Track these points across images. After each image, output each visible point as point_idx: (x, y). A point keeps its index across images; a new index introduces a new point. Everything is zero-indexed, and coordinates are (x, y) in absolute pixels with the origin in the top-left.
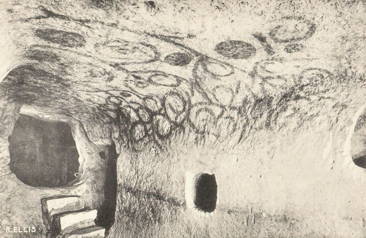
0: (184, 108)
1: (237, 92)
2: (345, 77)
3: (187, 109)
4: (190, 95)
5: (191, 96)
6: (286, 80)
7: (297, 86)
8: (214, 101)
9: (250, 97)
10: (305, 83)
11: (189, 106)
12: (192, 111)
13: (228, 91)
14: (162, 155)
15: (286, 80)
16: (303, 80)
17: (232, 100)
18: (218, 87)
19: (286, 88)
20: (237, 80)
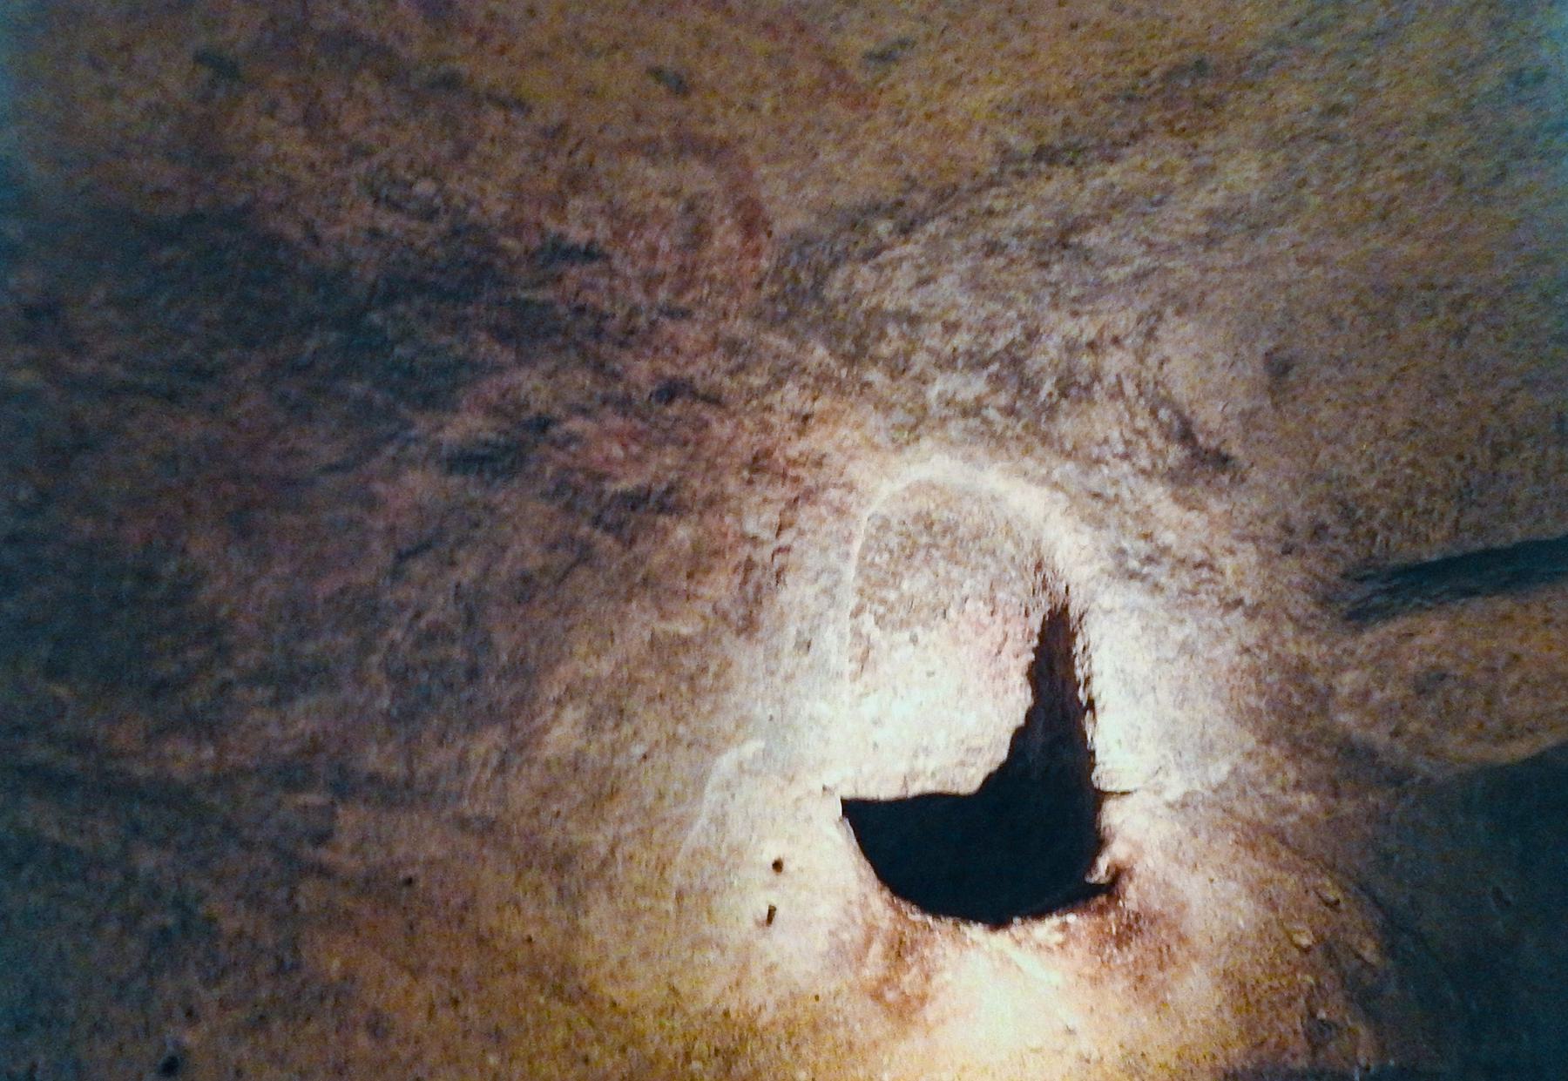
10: (577, 234)
15: (462, 153)
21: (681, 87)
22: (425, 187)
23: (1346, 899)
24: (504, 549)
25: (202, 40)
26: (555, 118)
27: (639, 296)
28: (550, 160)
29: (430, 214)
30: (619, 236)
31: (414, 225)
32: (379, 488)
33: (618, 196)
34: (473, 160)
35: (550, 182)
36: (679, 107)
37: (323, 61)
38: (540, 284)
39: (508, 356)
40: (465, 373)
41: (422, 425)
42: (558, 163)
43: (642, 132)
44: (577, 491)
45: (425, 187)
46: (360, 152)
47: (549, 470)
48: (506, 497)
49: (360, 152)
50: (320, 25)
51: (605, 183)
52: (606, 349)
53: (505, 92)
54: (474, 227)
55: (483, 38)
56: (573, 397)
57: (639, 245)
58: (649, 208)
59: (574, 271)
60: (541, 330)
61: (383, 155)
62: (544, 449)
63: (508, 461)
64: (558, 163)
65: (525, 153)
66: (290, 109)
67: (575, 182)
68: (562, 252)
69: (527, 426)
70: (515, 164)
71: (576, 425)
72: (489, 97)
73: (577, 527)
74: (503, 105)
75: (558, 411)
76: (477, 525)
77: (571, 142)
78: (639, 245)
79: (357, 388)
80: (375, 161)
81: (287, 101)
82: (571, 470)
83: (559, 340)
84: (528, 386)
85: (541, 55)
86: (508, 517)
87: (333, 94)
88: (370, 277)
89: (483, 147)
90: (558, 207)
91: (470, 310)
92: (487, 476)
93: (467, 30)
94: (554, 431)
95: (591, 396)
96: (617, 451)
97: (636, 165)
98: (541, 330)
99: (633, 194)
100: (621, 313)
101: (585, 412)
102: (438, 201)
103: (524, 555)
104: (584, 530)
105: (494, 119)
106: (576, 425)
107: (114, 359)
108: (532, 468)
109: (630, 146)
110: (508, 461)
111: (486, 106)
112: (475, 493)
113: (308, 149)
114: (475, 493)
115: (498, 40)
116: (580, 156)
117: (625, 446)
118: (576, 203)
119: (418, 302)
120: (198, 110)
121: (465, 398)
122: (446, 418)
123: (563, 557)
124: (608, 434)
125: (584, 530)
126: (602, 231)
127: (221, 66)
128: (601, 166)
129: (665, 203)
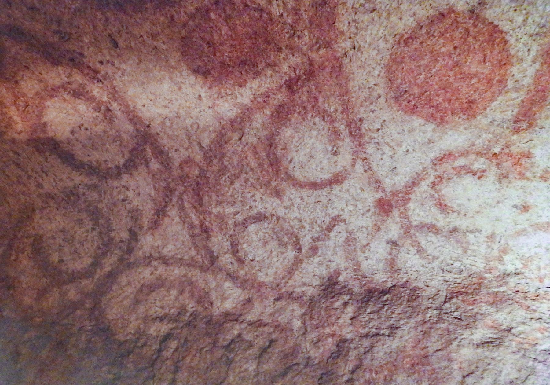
0: (96, 264)
1: (314, 250)
2: (103, 32)
3: (107, 269)
4: (146, 225)
5: (146, 225)
6: (465, 250)
7: (490, 271)
8: (226, 259)
9: (349, 276)
10: (510, 268)
11: (121, 260)
12: (123, 279)
13: (286, 239)
14: (403, 324)
15: (465, 250)
16: (507, 258)
17: (290, 273)
18: (260, 218)
19: (461, 272)
20: (330, 211)
21: (525, 208)
22: (457, 264)
23: (464, 125)
24: (501, 372)
25: (386, 237)
26: (489, 232)
27: (538, 284)
28: (493, 245)
29: (461, 272)
30: (525, 266)
31: (456, 276)
32: (453, 355)
33: (520, 251)
34: (469, 252)
35: (496, 253)
36: (527, 215)
37: (417, 234)
38: (501, 286)
39: (492, 310)
40: (479, 317)
41: (466, 334)
42: (496, 246)
43: (519, 227)
44: (525, 350)
45: (457, 264)
46: (435, 258)
47: (514, 344)
48: (498, 353)
49: (435, 258)
50: (414, 223)
51: (513, 248)
52: (528, 302)
53: (471, 228)
54: (475, 273)
55: (459, 213)
56: (519, 319)
57: (534, 267)
58: (533, 254)
59: (512, 280)
60: (504, 299)
61: (442, 258)
62: (511, 337)
63: (498, 342)
64: (496, 246)
65: (485, 246)
66: (413, 250)
67: (504, 251)
68: (506, 275)
69: (505, 330)
70: (483, 250)
71: (521, 328)
72: (468, 231)
73: (528, 363)
74: (471, 232)
75: (513, 325)
76: (489, 364)
77: (498, 239)
78: (534, 267)
79: (443, 326)
80: (440, 260)
81: (411, 248)
82: (522, 343)
83: (511, 302)
84: (502, 317)
85: (478, 212)
86: (500, 361)
87: (423, 243)
88: (445, 294)
89: (471, 247)
90: (500, 259)
91: (478, 297)
92: (491, 348)
93: (453, 211)
94: (513, 331)
95: (526, 318)
96: (539, 335)
97: (522, 239)
98: (504, 299)
99: (525, 249)
100: (533, 290)
101: (524, 323)
102: (462, 267)
103: (509, 374)
104: (531, 363)
105: (471, 236)
106: (521, 328)
107: (372, 328)
108: (507, 344)
109: (518, 233)
110: (498, 342)
111: (467, 233)
112: (487, 354)
113: (421, 261)
114: (487, 354)
115: (463, 212)
116: (503, 242)
117: (542, 333)
118: (507, 258)
119: (460, 298)
120: (389, 257)
121: (480, 324)
122: (474, 331)
123: (524, 373)
124: (534, 330)
125: (531, 363)
126: (519, 265)
127: (394, 244)
128: (511, 243)
129: (537, 250)
